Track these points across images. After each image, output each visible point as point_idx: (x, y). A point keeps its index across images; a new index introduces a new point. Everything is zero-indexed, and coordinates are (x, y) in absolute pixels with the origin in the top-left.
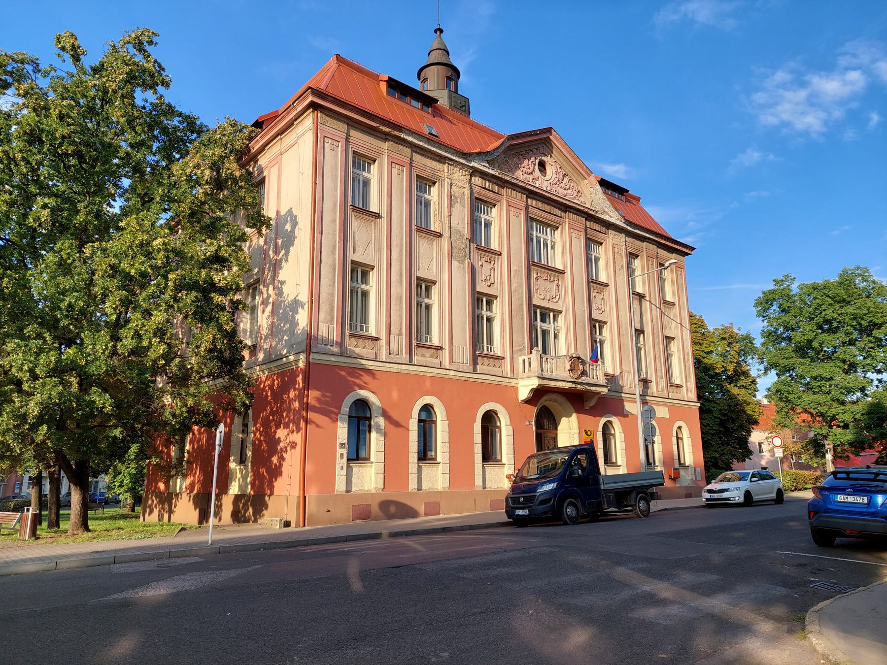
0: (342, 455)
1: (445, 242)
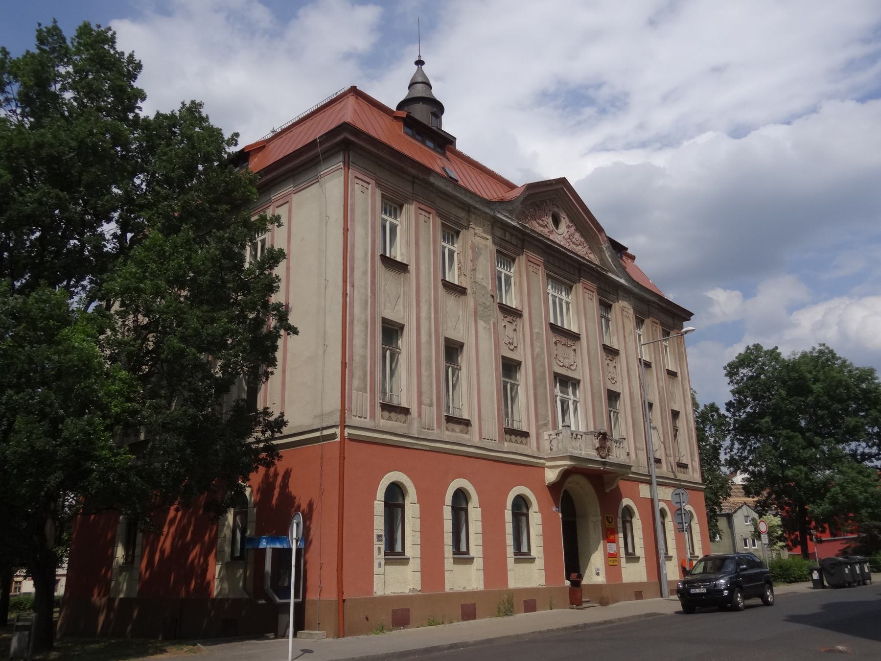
0: (379, 548)
1: (470, 299)
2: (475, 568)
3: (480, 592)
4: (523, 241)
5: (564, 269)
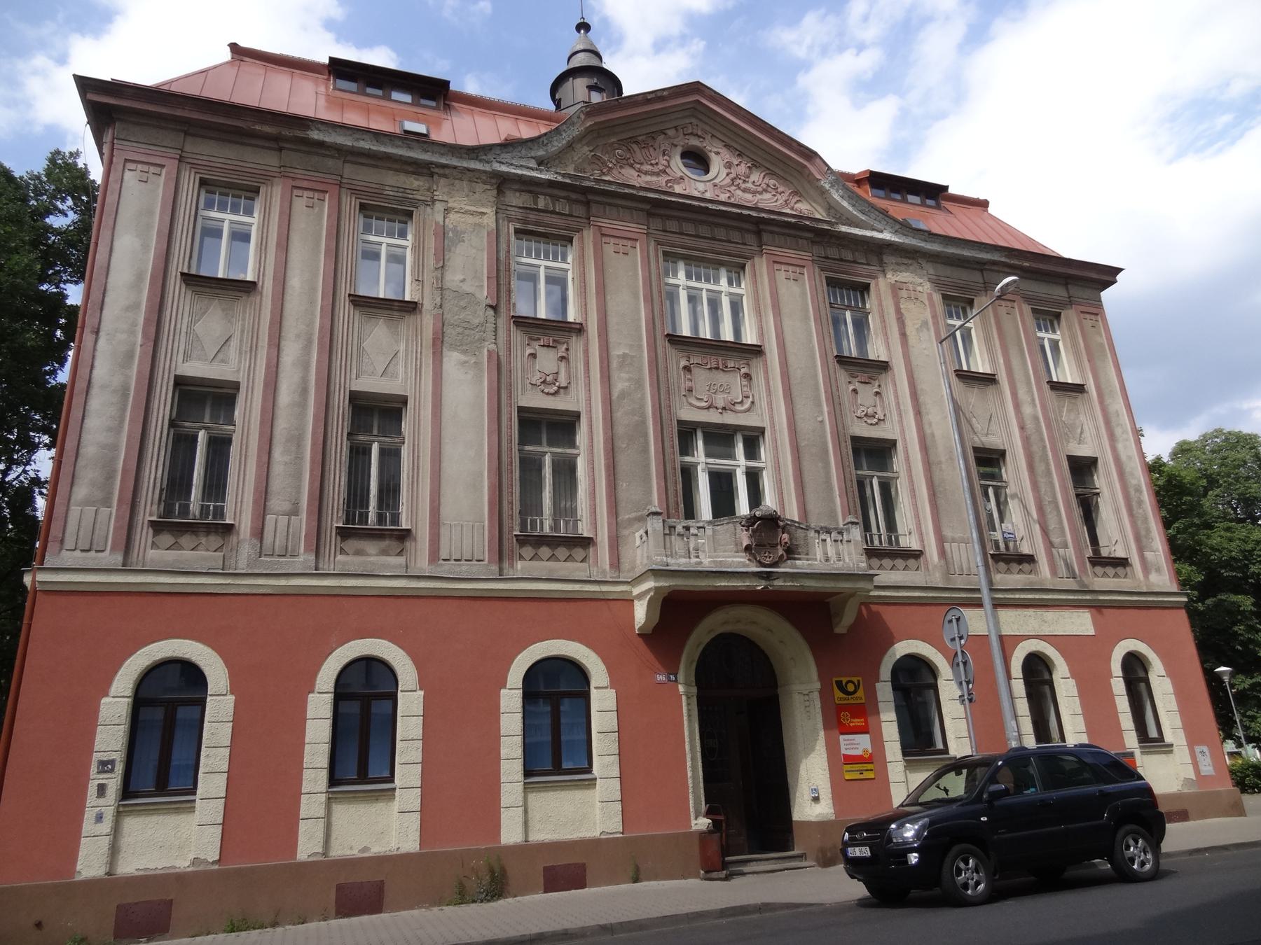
1: (427, 321)
2: (196, 822)
3: (408, 856)
4: (587, 204)
5: (720, 237)
